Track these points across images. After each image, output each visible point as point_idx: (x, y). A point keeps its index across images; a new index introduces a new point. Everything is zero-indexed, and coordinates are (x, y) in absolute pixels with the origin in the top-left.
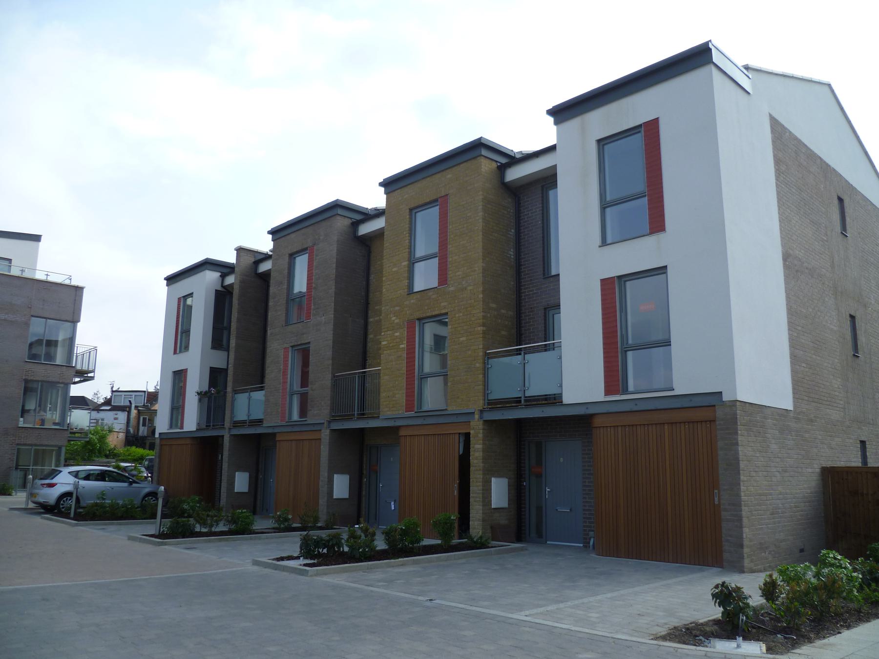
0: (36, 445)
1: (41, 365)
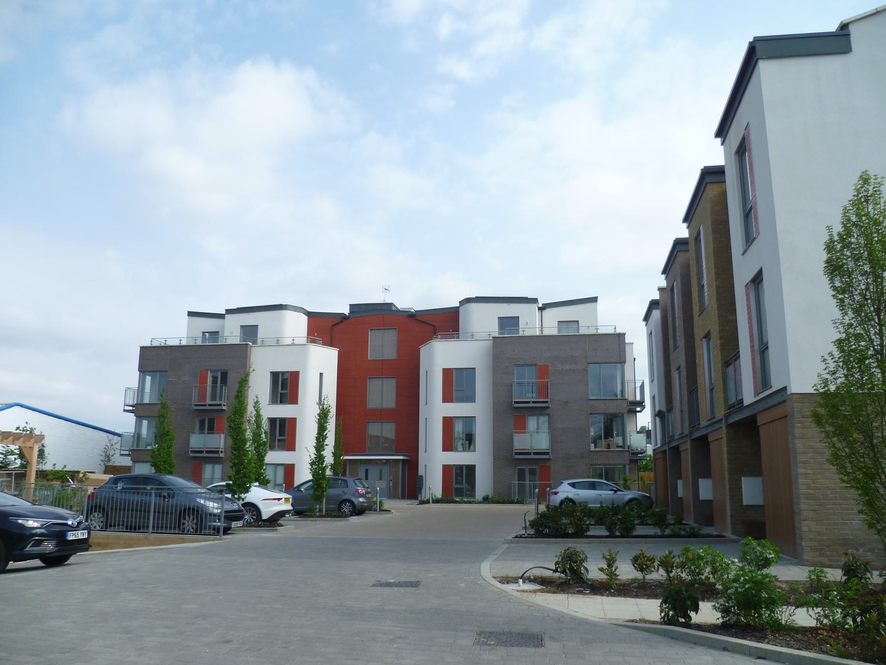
0: (605, 465)
1: (601, 401)
